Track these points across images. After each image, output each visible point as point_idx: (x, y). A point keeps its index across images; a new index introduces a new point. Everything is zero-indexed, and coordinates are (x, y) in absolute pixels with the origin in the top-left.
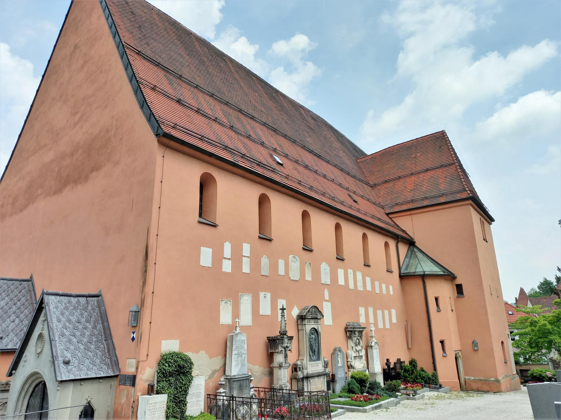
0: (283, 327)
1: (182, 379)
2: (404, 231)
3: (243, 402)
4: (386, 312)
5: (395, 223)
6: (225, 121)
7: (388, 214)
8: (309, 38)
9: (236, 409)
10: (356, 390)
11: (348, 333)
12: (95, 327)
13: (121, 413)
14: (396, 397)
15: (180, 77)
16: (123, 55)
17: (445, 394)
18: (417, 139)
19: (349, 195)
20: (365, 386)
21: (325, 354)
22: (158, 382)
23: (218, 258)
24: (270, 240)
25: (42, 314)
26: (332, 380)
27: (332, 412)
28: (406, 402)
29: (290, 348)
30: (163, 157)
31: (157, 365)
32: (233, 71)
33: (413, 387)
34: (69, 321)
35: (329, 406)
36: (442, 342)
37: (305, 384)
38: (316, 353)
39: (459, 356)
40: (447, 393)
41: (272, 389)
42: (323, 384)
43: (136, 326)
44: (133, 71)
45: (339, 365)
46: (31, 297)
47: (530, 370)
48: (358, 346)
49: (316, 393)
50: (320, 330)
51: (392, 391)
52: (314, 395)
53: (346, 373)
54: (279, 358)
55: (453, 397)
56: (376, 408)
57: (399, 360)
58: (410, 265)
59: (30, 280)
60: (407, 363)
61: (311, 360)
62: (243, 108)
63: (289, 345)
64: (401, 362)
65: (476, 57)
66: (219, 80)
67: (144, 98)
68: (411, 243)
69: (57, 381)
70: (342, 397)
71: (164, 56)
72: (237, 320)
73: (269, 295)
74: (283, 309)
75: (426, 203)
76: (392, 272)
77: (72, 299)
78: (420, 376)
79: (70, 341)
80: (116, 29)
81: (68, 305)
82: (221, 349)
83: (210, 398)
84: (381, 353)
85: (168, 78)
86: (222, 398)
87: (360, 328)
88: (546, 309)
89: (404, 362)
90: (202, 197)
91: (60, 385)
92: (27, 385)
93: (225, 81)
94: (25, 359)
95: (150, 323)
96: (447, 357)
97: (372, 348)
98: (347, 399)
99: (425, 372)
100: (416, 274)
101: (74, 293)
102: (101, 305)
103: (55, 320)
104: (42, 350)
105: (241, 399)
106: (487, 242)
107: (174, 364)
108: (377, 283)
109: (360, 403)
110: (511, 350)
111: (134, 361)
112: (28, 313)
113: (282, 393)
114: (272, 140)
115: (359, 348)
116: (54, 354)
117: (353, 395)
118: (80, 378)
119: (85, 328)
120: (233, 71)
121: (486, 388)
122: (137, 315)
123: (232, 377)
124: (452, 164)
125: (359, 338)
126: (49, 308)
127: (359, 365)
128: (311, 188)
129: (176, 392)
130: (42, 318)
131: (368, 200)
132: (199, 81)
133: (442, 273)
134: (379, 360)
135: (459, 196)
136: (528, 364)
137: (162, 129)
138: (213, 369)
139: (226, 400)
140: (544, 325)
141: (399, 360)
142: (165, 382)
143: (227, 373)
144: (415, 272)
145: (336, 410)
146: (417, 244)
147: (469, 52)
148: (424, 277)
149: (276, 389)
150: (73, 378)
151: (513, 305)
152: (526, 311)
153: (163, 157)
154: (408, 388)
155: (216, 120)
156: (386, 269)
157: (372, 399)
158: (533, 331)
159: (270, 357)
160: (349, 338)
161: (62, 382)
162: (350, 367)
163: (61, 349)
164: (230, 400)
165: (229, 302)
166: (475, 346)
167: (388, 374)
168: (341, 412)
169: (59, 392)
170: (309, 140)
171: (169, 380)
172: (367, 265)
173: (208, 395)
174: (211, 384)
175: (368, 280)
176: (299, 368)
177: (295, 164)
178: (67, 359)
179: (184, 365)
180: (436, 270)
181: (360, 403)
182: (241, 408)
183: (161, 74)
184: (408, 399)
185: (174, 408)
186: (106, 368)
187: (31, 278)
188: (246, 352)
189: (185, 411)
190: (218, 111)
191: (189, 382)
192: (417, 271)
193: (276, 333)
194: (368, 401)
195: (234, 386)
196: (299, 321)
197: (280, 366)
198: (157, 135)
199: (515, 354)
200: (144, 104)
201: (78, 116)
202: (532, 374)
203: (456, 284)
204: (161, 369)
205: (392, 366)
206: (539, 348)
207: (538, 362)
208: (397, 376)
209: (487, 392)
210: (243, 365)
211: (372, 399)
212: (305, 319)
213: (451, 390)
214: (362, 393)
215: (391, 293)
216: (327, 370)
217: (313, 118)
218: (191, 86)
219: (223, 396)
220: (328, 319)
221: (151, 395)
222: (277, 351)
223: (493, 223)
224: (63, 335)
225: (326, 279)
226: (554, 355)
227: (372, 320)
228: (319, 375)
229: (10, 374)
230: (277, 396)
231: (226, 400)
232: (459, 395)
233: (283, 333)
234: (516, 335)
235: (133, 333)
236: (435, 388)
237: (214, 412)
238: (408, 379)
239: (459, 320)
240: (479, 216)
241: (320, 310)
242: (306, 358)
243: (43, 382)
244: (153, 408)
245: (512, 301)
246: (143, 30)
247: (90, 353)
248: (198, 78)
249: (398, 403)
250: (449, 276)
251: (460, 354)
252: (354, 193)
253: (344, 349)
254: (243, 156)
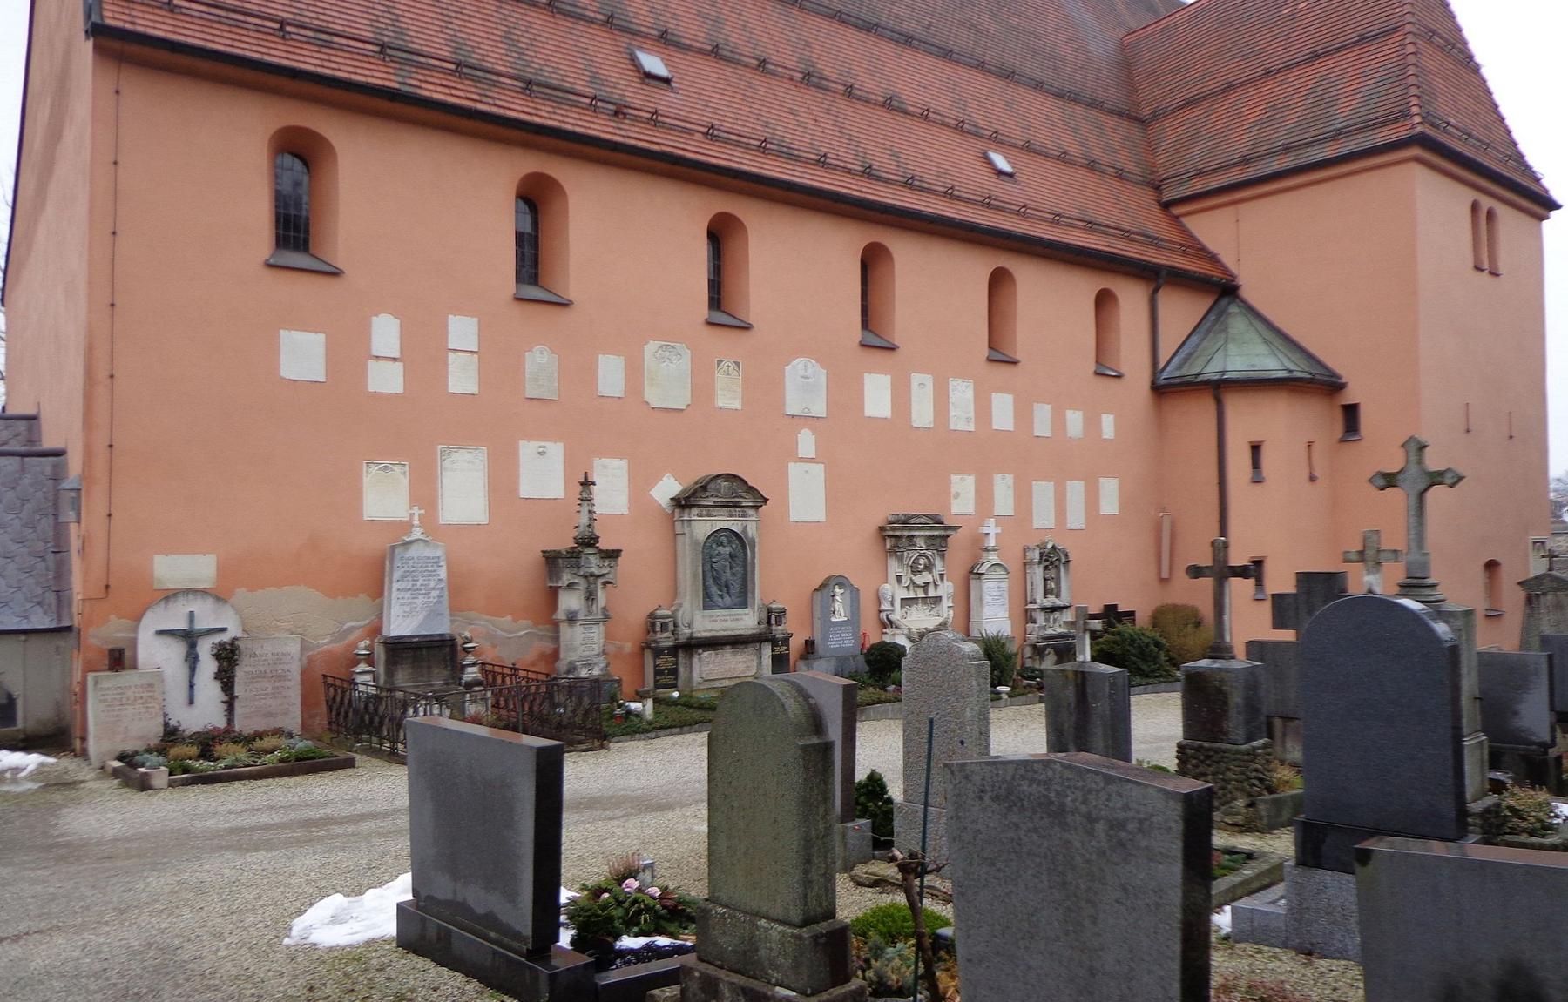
11: (888, 540)
29: (609, 578)
37: (681, 660)
45: (833, 619)
58: (1196, 354)
146: (1247, 293)
148: (1220, 388)
153: (117, 92)
180: (1270, 362)
197: (572, 619)
203: (1344, 403)
241: (750, 484)
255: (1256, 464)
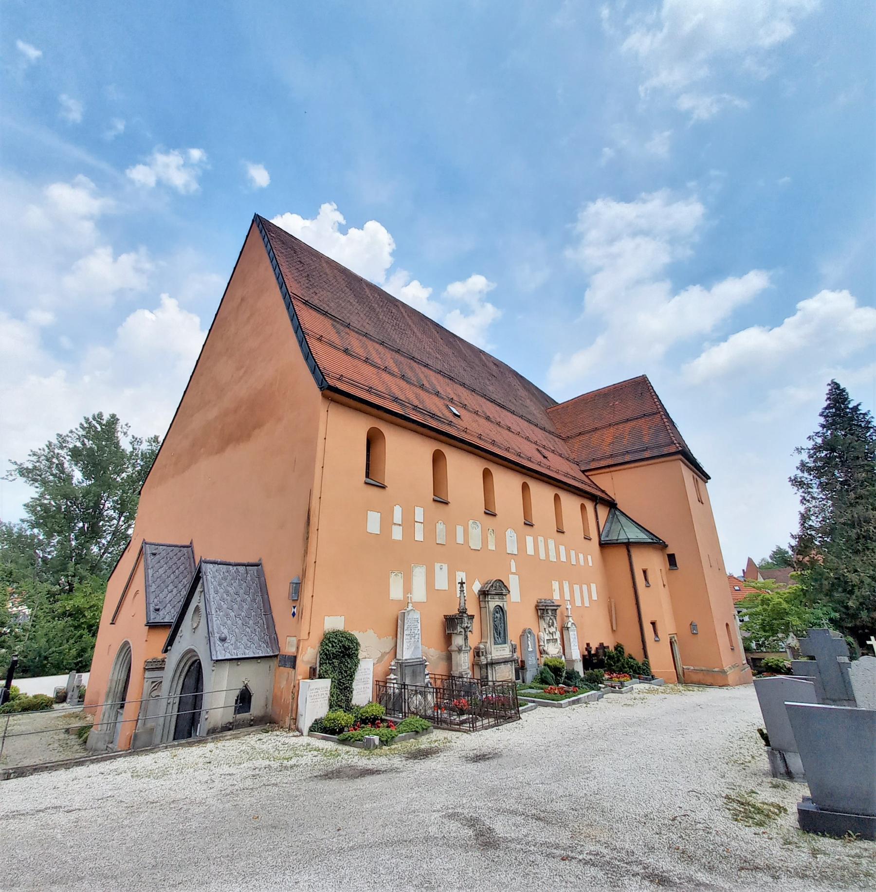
0: (462, 604)
1: (347, 662)
2: (603, 491)
3: (416, 691)
4: (585, 587)
5: (592, 481)
6: (396, 370)
7: (583, 472)
8: (487, 278)
9: (408, 699)
10: (550, 680)
12: (254, 600)
13: (281, 698)
14: (599, 689)
15: (348, 326)
16: (289, 305)
17: (658, 687)
18: (614, 385)
19: (538, 450)
20: (561, 676)
21: (513, 635)
22: (321, 664)
23: (387, 522)
24: (447, 503)
25: (200, 585)
26: (521, 668)
27: (521, 706)
28: (611, 695)
30: (327, 411)
31: (319, 645)
32: (406, 316)
33: (619, 678)
34: (227, 593)
35: (517, 699)
36: (653, 624)
37: (489, 671)
38: (502, 635)
39: (675, 640)
40: (660, 686)
41: (450, 677)
42: (511, 673)
43: (297, 600)
44: (299, 322)
46: (190, 565)
47: (764, 659)
48: (552, 627)
49: (501, 683)
50: (506, 608)
51: (593, 682)
52: (499, 686)
53: (538, 659)
54: (458, 641)
55: (669, 691)
56: (574, 702)
57: (601, 644)
58: (611, 531)
59: (190, 546)
60: (612, 648)
61: (495, 643)
62: (416, 355)
63: (469, 625)
64: (605, 647)
65: (675, 292)
66: (390, 327)
67: (310, 349)
68: (611, 505)
69: (212, 660)
70: (533, 688)
71: (332, 304)
72: (409, 595)
73: (445, 567)
74: (462, 583)
75: (628, 458)
76: (532, 526)
77: (231, 567)
78: (627, 664)
79: (227, 615)
80: (283, 279)
81: (227, 574)
82: (390, 628)
83: (379, 686)
84: (580, 638)
85: (335, 327)
86: (392, 685)
87: (553, 606)
88: (782, 584)
89: (608, 647)
90: (369, 455)
91: (215, 665)
92: (182, 664)
93: (397, 327)
94: (181, 635)
95: (312, 596)
96: (660, 642)
97: (568, 630)
98: (539, 691)
99: (634, 659)
100: (619, 541)
101: (232, 561)
102: (261, 575)
103: (212, 591)
104: (198, 625)
105: (414, 688)
106: (702, 503)
107: (338, 644)
108: (573, 553)
109: (554, 696)
110: (739, 636)
111: (294, 640)
112: (186, 583)
113: (462, 682)
114: (448, 389)
115: (552, 629)
116: (210, 629)
117: (547, 686)
118: (236, 657)
119: (244, 601)
120: (406, 316)
121: (709, 680)
122: (297, 589)
123: (403, 662)
124: (656, 413)
125: (552, 617)
126: (206, 577)
127: (553, 650)
128: (493, 443)
129: (340, 677)
130: (199, 589)
131: (560, 455)
132: (370, 329)
133: (650, 541)
134: (577, 644)
135: (666, 450)
136: (762, 652)
137: (326, 381)
138: (383, 651)
139: (397, 688)
140: (780, 604)
141: (601, 644)
142: (328, 665)
143: (398, 657)
144: (617, 540)
145: (526, 704)
146: (619, 506)
147: (667, 285)
148: (628, 545)
149: (454, 677)
150: (230, 657)
151: (739, 579)
152: (755, 585)
153: (327, 411)
154: (613, 679)
155: (385, 369)
156: (583, 536)
157: (569, 692)
158: (765, 610)
159: (448, 639)
160: (541, 617)
161: (217, 661)
162: (543, 652)
163: (217, 624)
164: (402, 689)
165: (400, 575)
166: (694, 629)
167: (589, 661)
168: (532, 706)
169: (214, 672)
170: (491, 388)
171: (333, 663)
172: (560, 531)
173: (377, 681)
174: (381, 669)
175: (562, 549)
176: (482, 652)
177: (475, 415)
178: (223, 636)
179: (349, 646)
180: (642, 536)
181: (554, 696)
182: (414, 698)
183: (327, 322)
184: (612, 692)
185: (339, 695)
186: (265, 646)
187: (191, 543)
188: (419, 632)
189: (351, 699)
190: (389, 359)
191: (355, 666)
192: (619, 538)
193: (454, 611)
194: (564, 694)
195: (406, 672)
196: (481, 597)
197: (460, 650)
198: (321, 388)
199: (745, 639)
200: (308, 355)
201: (243, 371)
202: (767, 664)
204: (323, 650)
205: (593, 652)
206: (775, 633)
207: (774, 650)
208: (600, 664)
209: (711, 685)
210: (416, 648)
211: (569, 692)
212: (488, 594)
213: (666, 682)
214: (558, 684)
215: (590, 564)
216: (515, 656)
217: (495, 364)
218: (360, 334)
219: (394, 683)
220: (515, 595)
221: (312, 679)
222: (455, 632)
223: (709, 481)
224: (219, 608)
225: (512, 547)
226: (792, 641)
227: (567, 596)
228: (505, 662)
229: (166, 651)
230: (456, 684)
231: (397, 688)
232: (676, 688)
233: (463, 611)
234: (745, 615)
235: (294, 607)
236: (646, 679)
237: (383, 702)
238: (613, 667)
239: (672, 596)
240: (692, 473)
241: (505, 584)
242: (490, 642)
243: (198, 661)
244: (316, 694)
245: (738, 573)
246: (311, 279)
247: (248, 629)
248: (367, 326)
249: (601, 697)
250: (658, 544)
251: (676, 638)
252: (544, 447)
253: (535, 631)
254: (415, 408)
255: (135, 596)
